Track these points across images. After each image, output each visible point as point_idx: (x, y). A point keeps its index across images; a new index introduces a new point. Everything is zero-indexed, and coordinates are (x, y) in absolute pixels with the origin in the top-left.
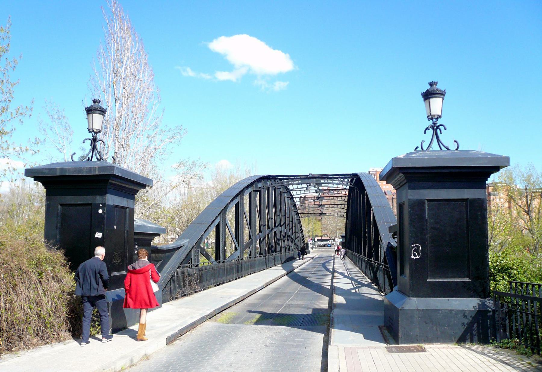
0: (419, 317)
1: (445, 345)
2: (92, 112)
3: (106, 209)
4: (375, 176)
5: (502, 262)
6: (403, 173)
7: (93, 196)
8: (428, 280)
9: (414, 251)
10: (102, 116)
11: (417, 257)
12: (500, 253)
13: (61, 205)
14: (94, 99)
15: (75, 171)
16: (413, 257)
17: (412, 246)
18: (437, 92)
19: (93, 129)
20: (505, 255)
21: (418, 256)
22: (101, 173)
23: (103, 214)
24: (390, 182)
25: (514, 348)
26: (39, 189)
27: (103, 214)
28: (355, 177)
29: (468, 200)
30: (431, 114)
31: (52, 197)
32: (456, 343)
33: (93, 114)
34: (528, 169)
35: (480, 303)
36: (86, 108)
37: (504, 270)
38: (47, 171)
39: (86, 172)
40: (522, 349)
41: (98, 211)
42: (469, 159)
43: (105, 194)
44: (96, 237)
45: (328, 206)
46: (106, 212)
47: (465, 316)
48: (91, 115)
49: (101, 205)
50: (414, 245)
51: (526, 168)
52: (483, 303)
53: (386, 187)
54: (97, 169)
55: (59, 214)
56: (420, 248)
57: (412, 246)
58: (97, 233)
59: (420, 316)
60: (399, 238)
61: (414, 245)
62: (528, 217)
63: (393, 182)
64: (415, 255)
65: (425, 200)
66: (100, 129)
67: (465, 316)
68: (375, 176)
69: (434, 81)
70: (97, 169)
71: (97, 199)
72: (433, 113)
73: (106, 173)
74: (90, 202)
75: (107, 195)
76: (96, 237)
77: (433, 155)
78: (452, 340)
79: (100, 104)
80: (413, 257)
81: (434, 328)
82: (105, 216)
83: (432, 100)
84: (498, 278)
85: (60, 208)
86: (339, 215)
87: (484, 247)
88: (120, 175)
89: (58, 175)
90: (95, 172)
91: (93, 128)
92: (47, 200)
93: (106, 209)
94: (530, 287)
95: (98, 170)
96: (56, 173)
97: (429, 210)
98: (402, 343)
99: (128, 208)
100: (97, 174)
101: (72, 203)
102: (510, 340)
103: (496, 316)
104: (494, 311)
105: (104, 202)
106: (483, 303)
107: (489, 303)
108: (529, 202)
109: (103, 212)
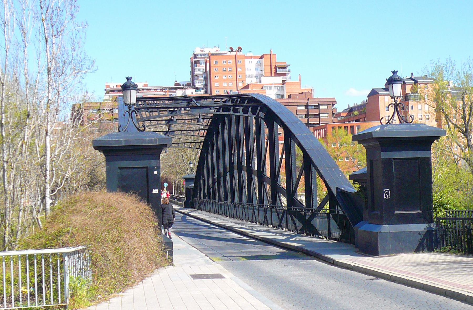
0: (391, 237)
1: (406, 254)
4: (208, 64)
5: (441, 199)
6: (378, 141)
8: (395, 213)
9: (385, 194)
11: (388, 198)
12: (439, 194)
16: (385, 198)
17: (385, 190)
18: (398, 80)
20: (442, 195)
21: (389, 197)
24: (365, 143)
25: (449, 251)
26: (101, 156)
27: (158, 174)
28: (260, 105)
29: (420, 158)
30: (393, 95)
31: (112, 163)
32: (414, 252)
33: (131, 91)
34: (468, 66)
35: (428, 226)
37: (442, 205)
40: (454, 251)
41: (155, 171)
42: (422, 132)
44: (153, 193)
45: (180, 133)
47: (420, 234)
49: (156, 168)
50: (386, 190)
51: (464, 64)
52: (430, 226)
53: (228, 84)
56: (390, 192)
57: (385, 190)
58: (154, 190)
59: (392, 236)
61: (386, 190)
62: (465, 141)
63: (368, 144)
64: (386, 197)
65: (392, 159)
67: (420, 234)
68: (208, 64)
69: (396, 71)
72: (395, 95)
74: (146, 166)
76: (153, 193)
77: (398, 128)
78: (411, 251)
80: (385, 198)
81: (401, 244)
83: (394, 85)
84: (438, 210)
86: (192, 146)
87: (430, 190)
90: (156, 143)
92: (107, 165)
94: (457, 212)
96: (122, 144)
97: (394, 165)
98: (380, 255)
102: (446, 247)
103: (438, 233)
104: (436, 231)
106: (430, 226)
107: (433, 226)
108: (467, 117)
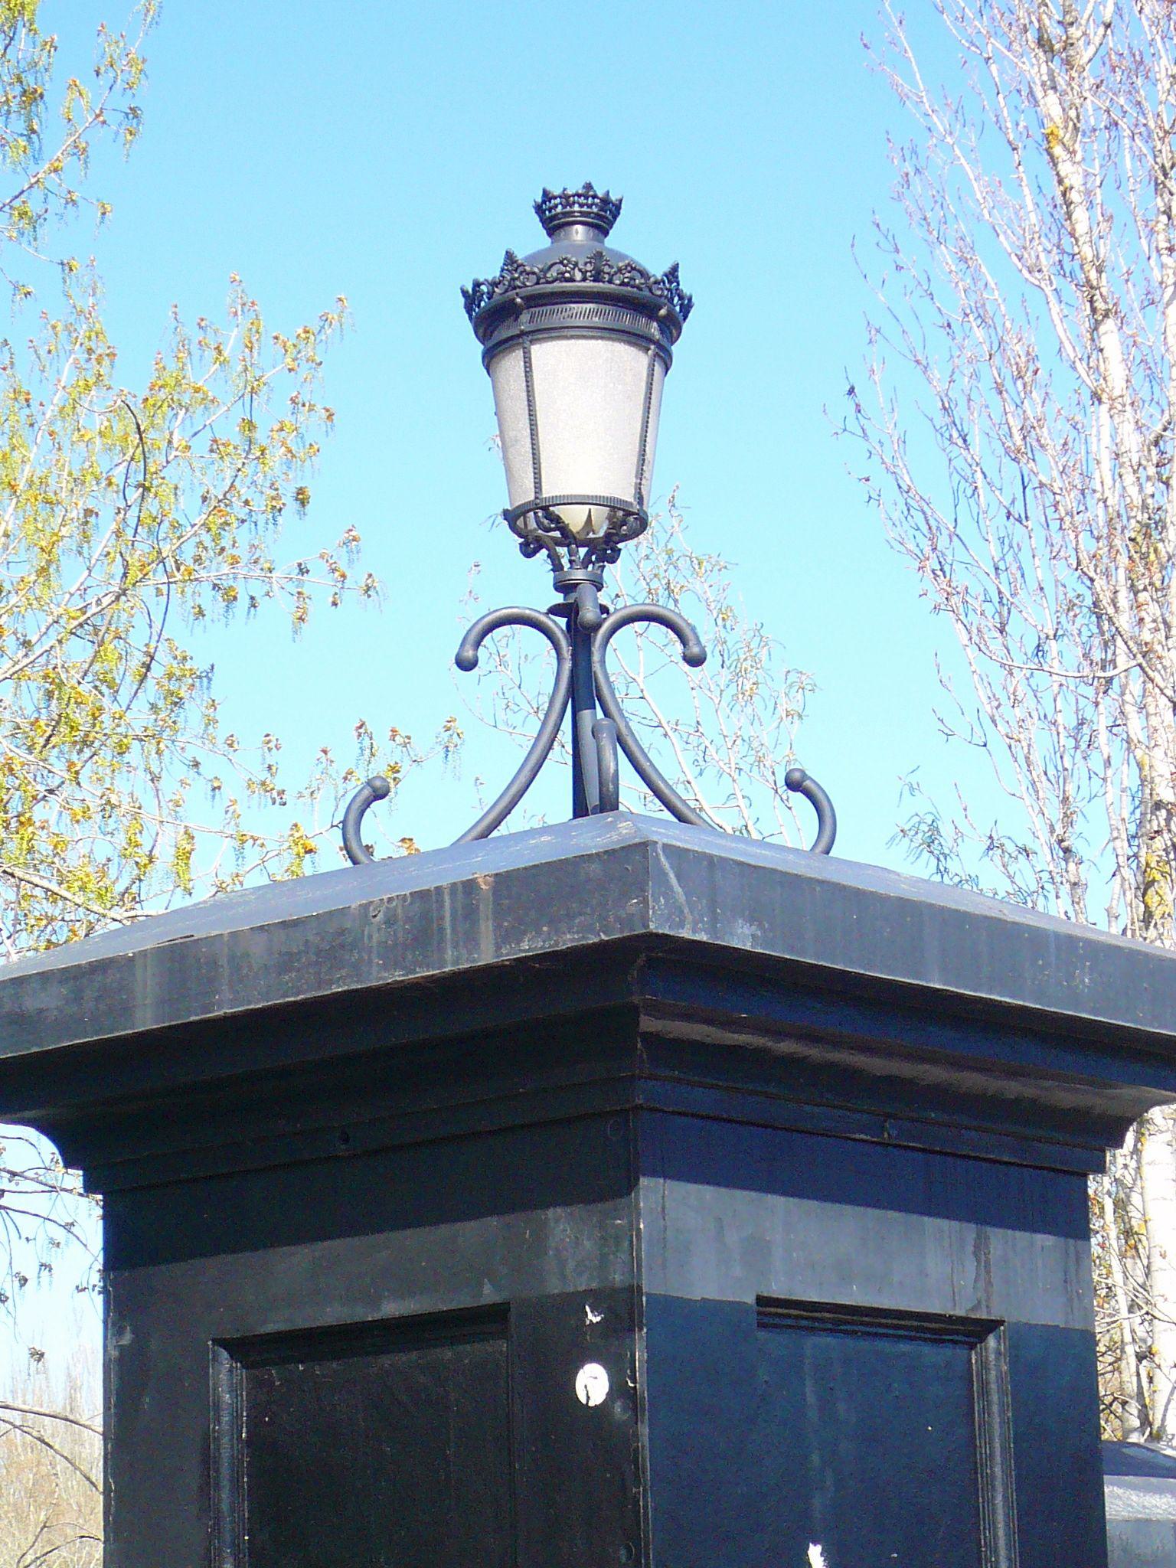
2: (524, 322)
3: (640, 1355)
7: (509, 1218)
10: (633, 360)
13: (243, 1348)
14: (547, 196)
15: (287, 963)
19: (545, 510)
22: (528, 946)
23: (618, 1408)
33: (537, 350)
36: (471, 299)
38: (49, 1001)
39: (392, 955)
43: (628, 1186)
46: (640, 1383)
48: (512, 364)
49: (593, 1318)
54: (486, 909)
55: (225, 1454)
60: (801, 868)
66: (628, 495)
70: (486, 909)
71: (552, 1243)
73: (567, 940)
74: (489, 1295)
75: (651, 1191)
79: (620, 240)
82: (644, 1430)
85: (233, 1390)
88: (742, 937)
89: (146, 1020)
90: (471, 940)
91: (548, 492)
93: (640, 1355)
95: (499, 914)
96: (126, 1010)
99: (992, 1326)
100: (486, 955)
101: (333, 1314)
105: (618, 1278)
109: (618, 1389)
